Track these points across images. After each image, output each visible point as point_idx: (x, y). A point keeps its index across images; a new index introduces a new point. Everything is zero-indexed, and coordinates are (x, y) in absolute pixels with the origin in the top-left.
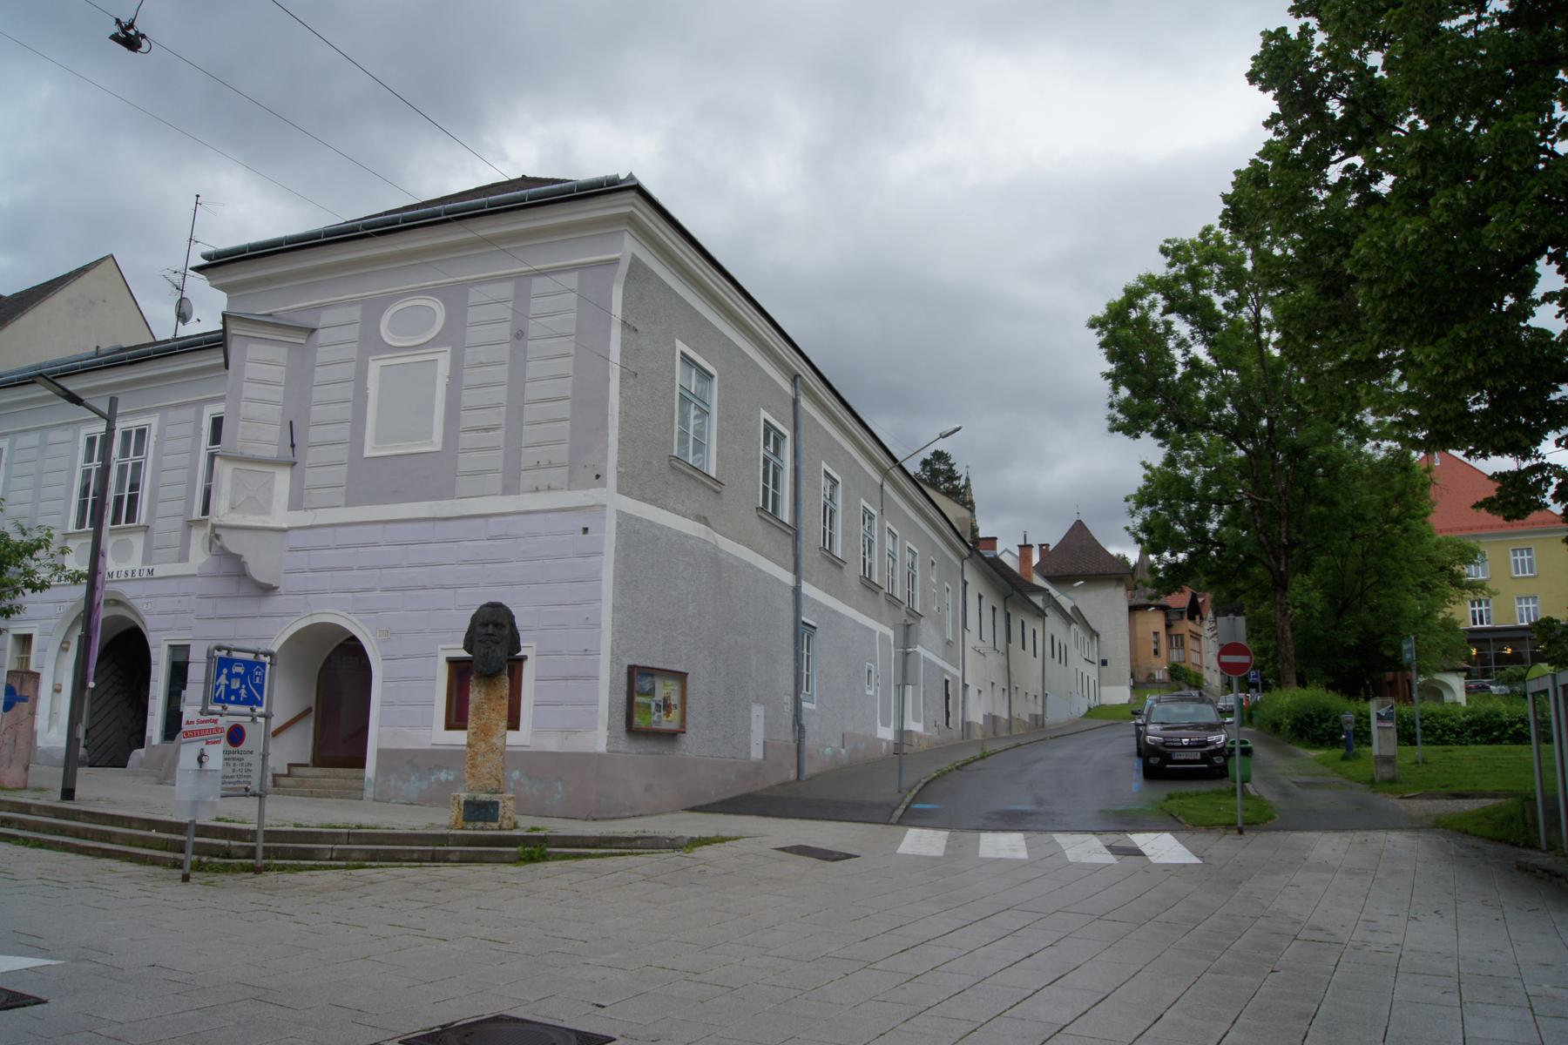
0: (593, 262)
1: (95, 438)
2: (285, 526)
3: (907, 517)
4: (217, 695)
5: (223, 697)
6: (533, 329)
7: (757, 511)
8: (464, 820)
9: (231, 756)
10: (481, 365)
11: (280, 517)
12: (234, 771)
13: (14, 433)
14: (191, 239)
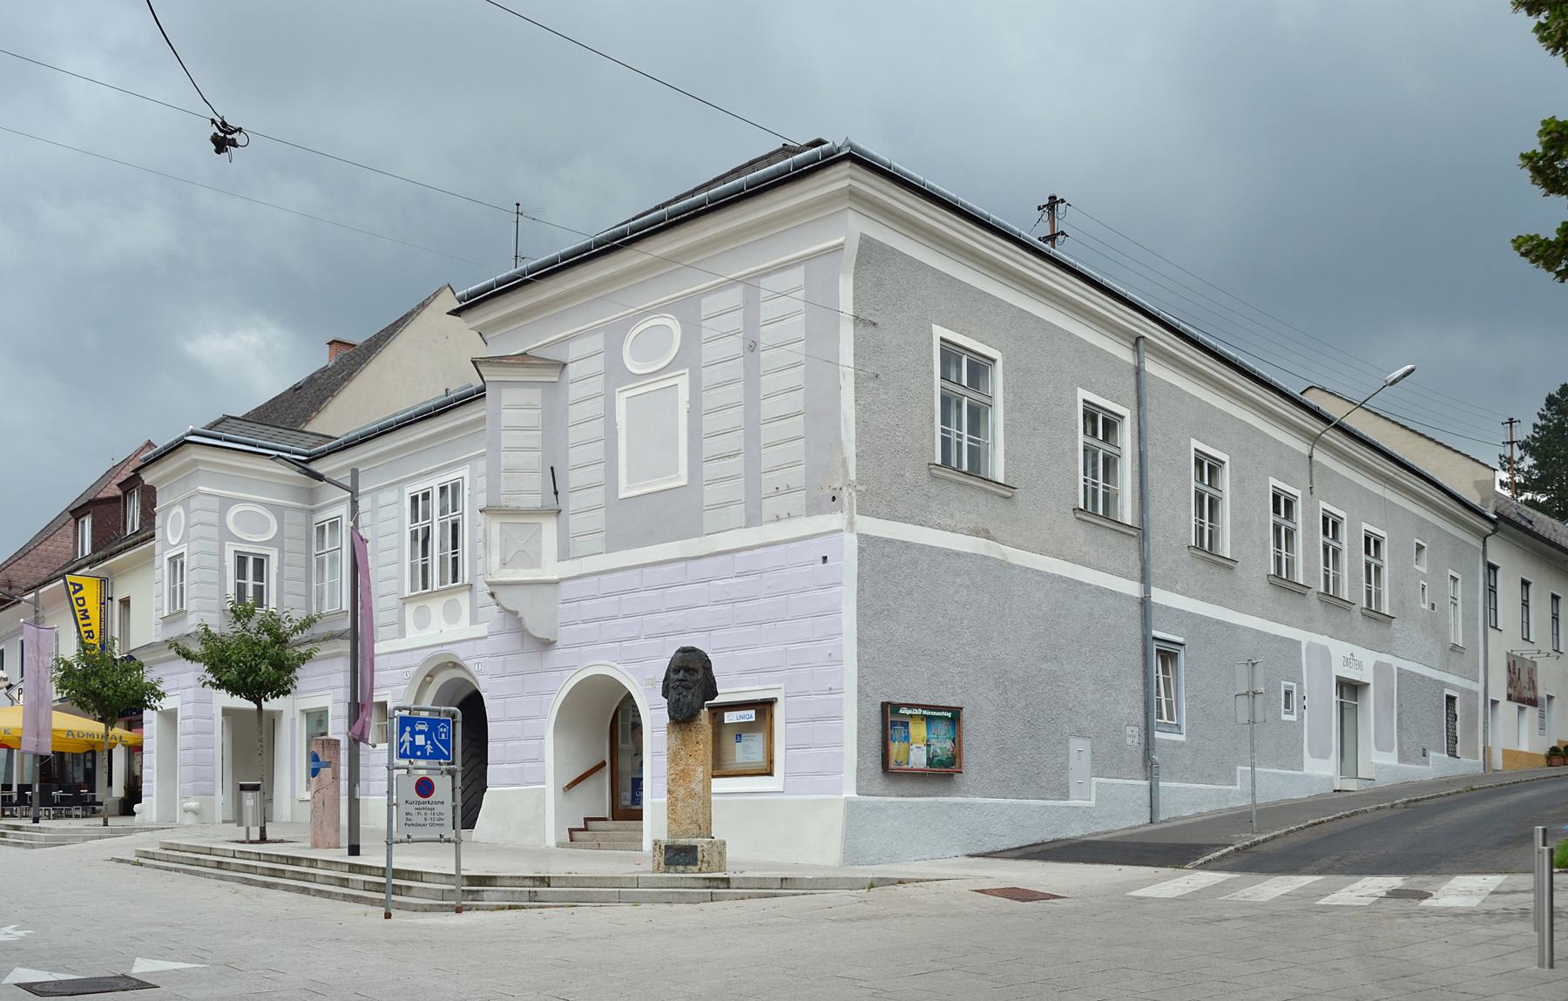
0: (818, 252)
1: (417, 496)
2: (556, 578)
3: (1360, 488)
4: (402, 751)
5: (408, 753)
6: (766, 336)
7: (1075, 513)
8: (666, 864)
9: (421, 806)
10: (718, 385)
11: (551, 569)
12: (426, 819)
13: (373, 490)
14: (517, 256)
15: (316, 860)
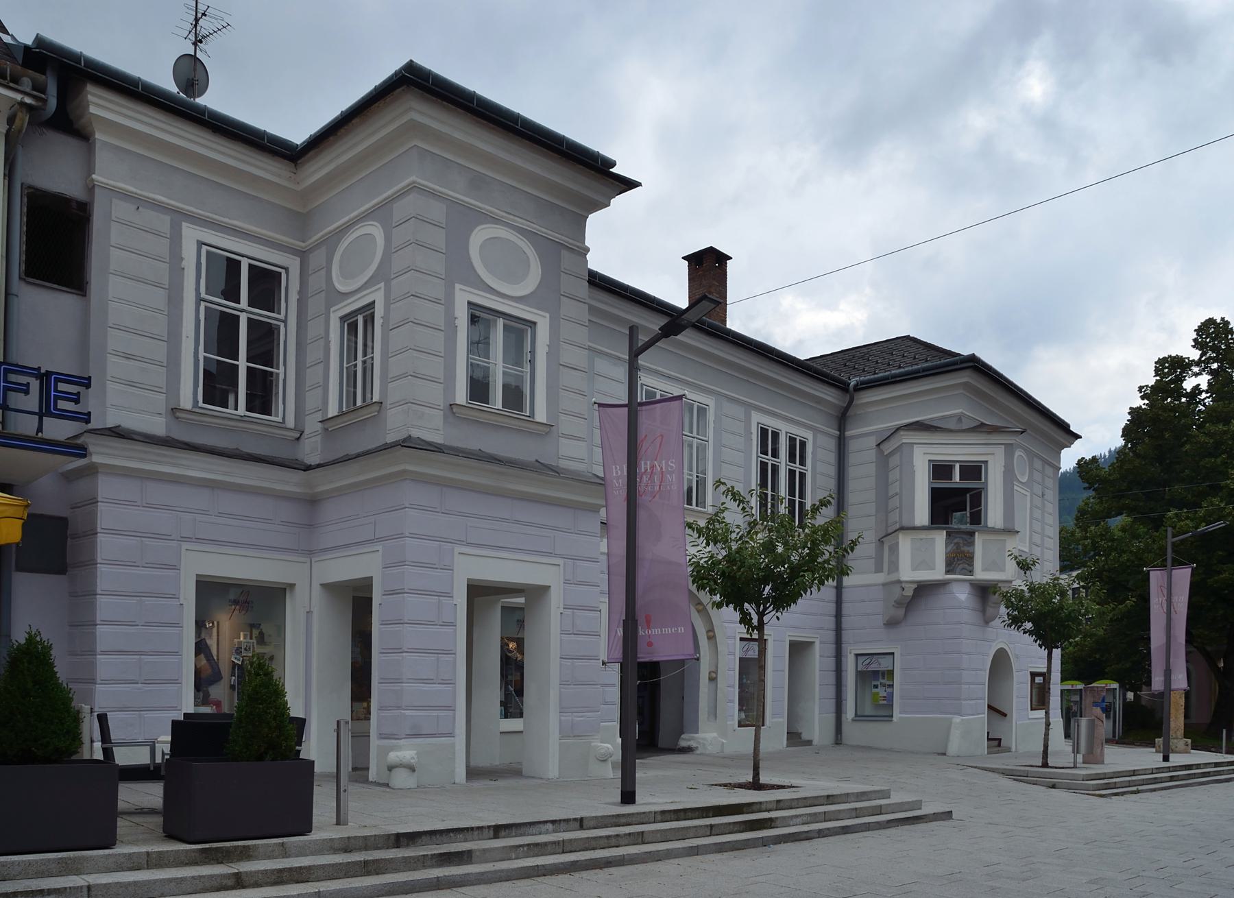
15: (1200, 764)
